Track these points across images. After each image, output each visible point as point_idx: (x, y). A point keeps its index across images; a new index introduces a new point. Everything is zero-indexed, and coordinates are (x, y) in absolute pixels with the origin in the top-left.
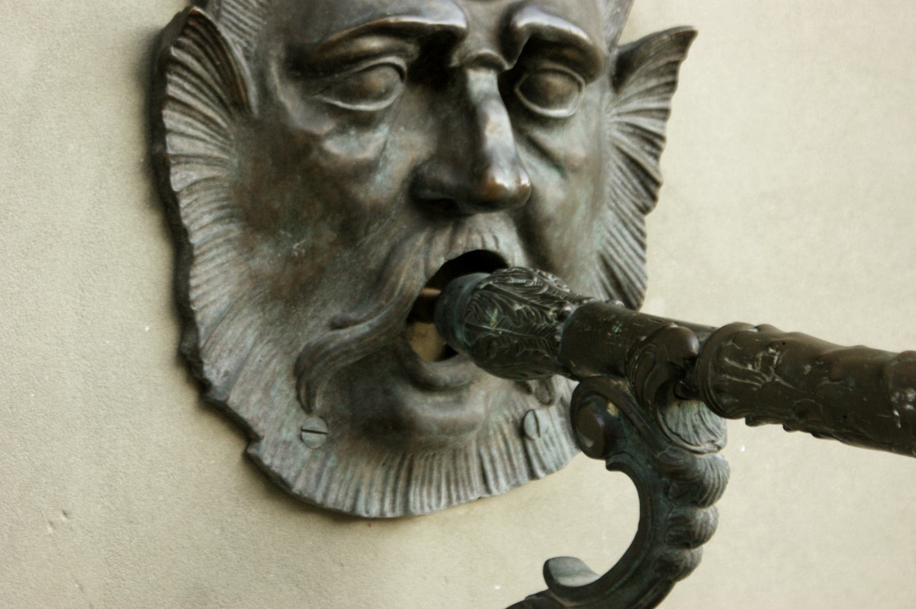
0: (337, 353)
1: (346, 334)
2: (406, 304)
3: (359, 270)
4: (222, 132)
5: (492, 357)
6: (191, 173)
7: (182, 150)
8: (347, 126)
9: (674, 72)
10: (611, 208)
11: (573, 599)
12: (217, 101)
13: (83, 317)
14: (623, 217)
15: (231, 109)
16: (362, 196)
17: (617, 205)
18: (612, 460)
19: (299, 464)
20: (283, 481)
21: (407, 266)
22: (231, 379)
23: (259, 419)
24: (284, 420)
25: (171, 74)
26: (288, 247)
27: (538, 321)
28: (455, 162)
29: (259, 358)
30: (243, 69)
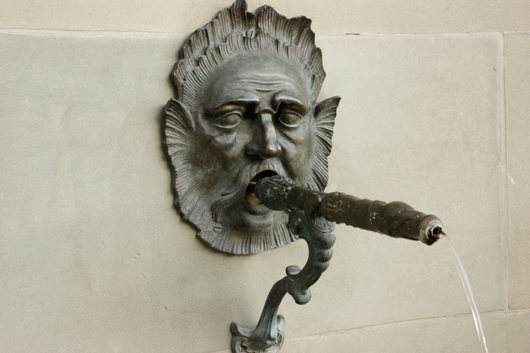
0: (224, 203)
1: (226, 197)
2: (244, 188)
3: (230, 177)
4: (184, 136)
5: (269, 204)
6: (175, 149)
7: (172, 142)
8: (223, 133)
9: (335, 111)
10: (315, 155)
11: (293, 279)
12: (182, 127)
13: (142, 194)
14: (320, 157)
15: (187, 129)
16: (228, 154)
17: (317, 153)
18: (300, 235)
19: (213, 238)
20: (208, 244)
21: (244, 176)
22: (190, 212)
23: (200, 224)
24: (208, 224)
25: (167, 119)
26: (206, 171)
27: (281, 192)
28: (258, 143)
29: (199, 205)
30: (190, 117)
